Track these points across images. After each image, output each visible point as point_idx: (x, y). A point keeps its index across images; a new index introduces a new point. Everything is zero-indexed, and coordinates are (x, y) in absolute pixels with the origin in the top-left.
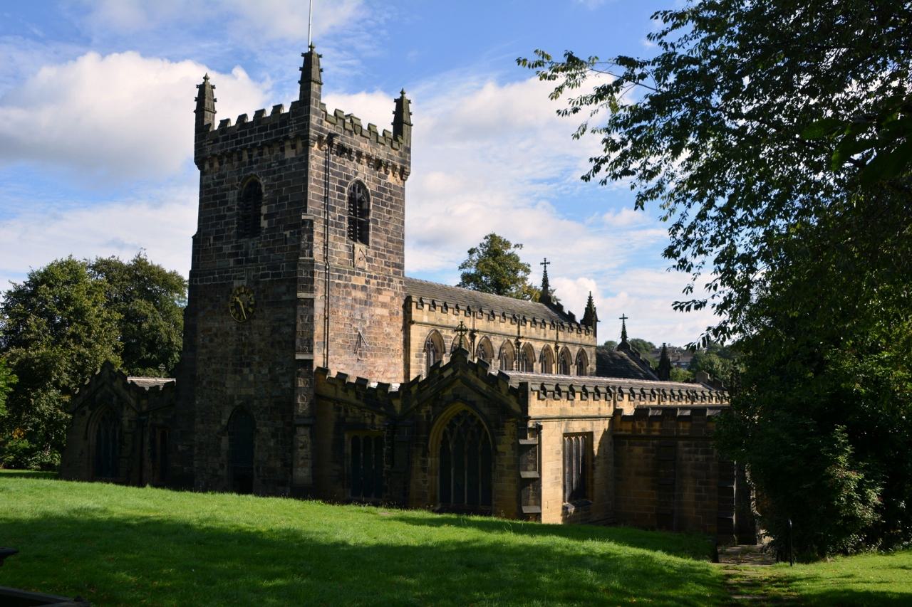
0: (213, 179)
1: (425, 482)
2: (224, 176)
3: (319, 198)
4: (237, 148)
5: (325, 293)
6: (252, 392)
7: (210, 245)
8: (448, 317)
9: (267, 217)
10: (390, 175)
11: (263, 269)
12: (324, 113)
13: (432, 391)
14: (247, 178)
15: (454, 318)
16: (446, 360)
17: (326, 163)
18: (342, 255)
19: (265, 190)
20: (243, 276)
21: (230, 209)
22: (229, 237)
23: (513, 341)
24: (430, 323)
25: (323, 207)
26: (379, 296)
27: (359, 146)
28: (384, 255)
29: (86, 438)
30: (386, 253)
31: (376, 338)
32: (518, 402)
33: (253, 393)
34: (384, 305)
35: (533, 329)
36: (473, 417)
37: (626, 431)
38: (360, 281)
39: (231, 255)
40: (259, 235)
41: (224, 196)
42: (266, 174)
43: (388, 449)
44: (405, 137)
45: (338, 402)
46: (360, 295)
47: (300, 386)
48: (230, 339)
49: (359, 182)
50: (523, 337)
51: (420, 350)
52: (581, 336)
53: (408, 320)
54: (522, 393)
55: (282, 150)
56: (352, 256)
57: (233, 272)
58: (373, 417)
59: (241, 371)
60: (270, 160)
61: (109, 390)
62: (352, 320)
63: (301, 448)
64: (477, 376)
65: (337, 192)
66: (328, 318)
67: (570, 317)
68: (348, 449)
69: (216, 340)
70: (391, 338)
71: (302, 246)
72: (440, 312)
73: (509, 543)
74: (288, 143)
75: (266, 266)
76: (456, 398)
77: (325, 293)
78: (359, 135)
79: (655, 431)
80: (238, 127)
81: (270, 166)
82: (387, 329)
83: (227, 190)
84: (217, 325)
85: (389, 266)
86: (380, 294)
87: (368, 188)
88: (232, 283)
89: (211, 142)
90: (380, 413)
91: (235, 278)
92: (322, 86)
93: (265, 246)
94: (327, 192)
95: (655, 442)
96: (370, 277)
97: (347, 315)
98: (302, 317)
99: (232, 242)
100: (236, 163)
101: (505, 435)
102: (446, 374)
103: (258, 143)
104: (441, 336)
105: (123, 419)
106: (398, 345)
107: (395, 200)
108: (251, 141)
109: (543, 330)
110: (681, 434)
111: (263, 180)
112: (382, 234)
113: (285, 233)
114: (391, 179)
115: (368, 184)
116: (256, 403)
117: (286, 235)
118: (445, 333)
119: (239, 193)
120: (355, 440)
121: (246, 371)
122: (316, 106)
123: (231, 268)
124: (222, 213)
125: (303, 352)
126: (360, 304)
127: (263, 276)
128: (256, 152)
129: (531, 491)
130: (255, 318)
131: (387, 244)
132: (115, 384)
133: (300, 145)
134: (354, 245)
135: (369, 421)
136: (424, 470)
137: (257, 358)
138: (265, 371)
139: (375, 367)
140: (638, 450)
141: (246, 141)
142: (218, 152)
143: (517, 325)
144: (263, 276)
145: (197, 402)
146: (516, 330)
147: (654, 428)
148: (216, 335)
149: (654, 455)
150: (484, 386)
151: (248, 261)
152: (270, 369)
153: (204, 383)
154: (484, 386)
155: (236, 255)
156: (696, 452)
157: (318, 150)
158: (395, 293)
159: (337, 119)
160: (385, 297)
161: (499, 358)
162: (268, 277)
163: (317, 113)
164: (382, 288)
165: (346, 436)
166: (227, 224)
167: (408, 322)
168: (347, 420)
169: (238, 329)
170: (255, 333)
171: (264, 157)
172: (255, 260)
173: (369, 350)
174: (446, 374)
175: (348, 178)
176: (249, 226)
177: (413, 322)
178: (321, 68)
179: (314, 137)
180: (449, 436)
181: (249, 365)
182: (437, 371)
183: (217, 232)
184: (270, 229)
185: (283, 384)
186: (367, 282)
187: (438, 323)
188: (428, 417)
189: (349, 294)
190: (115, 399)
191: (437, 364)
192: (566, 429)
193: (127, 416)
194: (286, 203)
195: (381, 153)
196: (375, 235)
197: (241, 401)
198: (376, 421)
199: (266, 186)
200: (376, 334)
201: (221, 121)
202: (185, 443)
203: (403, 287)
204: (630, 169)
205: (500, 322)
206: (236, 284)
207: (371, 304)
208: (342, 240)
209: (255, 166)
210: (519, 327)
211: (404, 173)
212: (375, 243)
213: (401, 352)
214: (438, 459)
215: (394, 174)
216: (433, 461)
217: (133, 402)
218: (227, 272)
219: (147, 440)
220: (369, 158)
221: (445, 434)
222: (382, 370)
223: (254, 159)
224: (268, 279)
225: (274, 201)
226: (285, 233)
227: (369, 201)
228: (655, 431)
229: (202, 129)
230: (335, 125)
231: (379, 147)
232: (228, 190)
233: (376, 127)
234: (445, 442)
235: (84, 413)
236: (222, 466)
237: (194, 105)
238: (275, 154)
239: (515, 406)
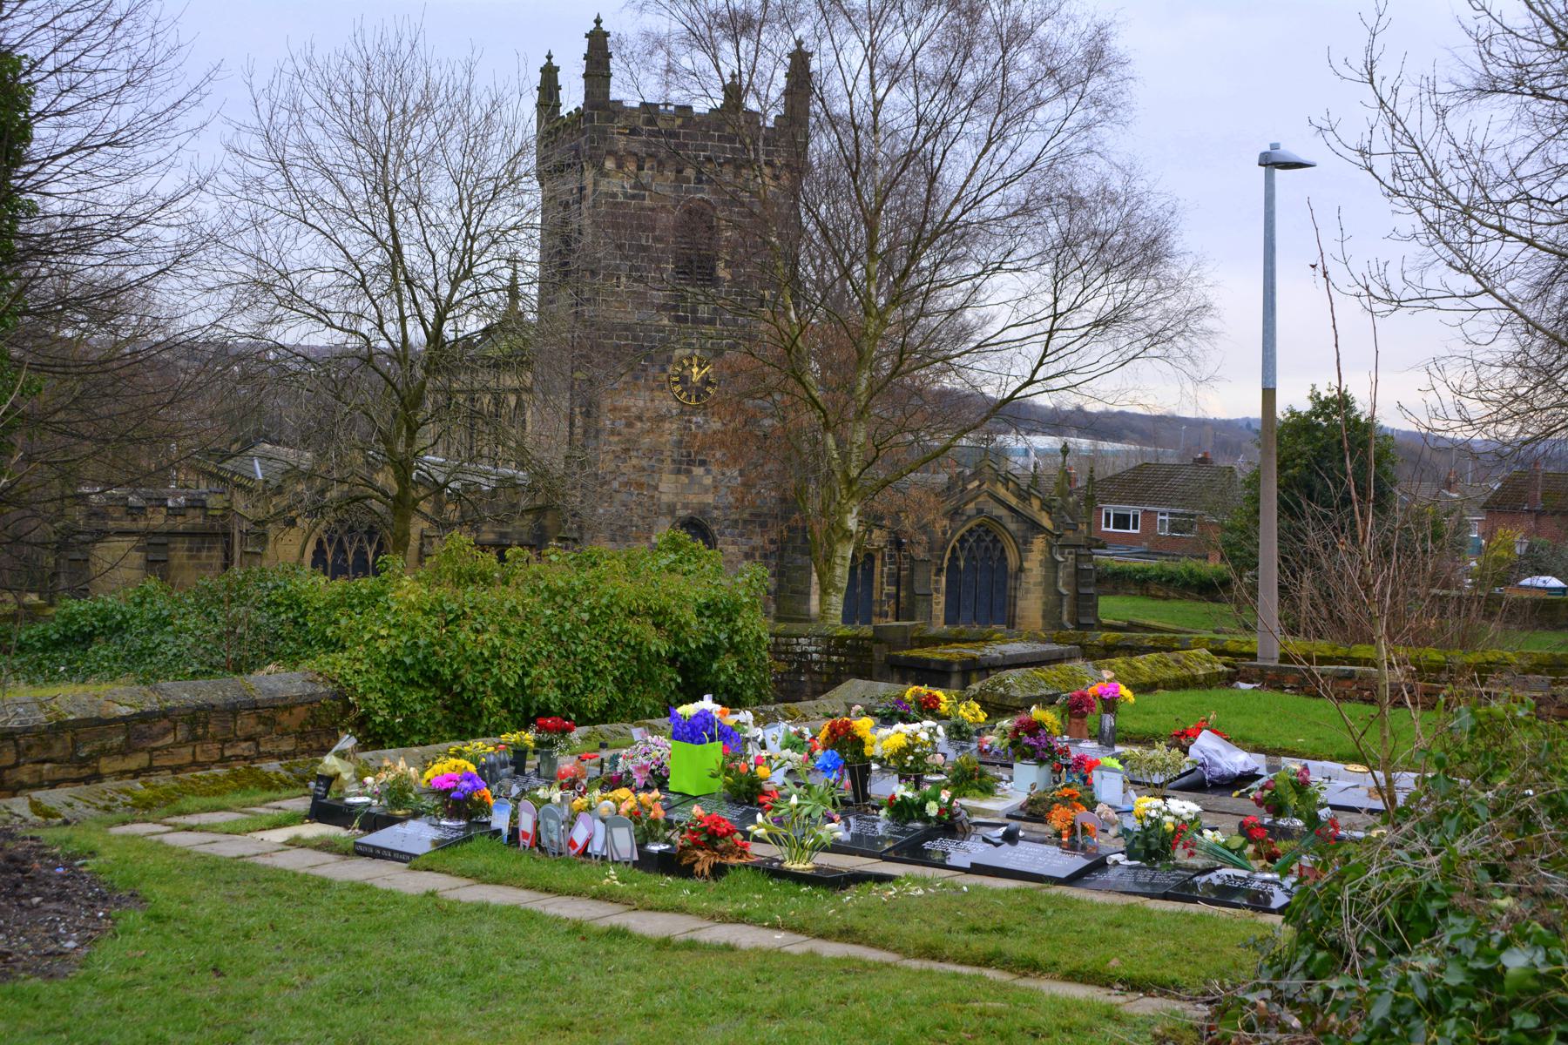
6: (709, 499)
39: (662, 307)
48: (667, 425)
59: (689, 472)
84: (641, 403)
116: (716, 513)
121: (698, 471)
155: (675, 308)
181: (703, 463)
188: (944, 533)
204: (1206, 1011)
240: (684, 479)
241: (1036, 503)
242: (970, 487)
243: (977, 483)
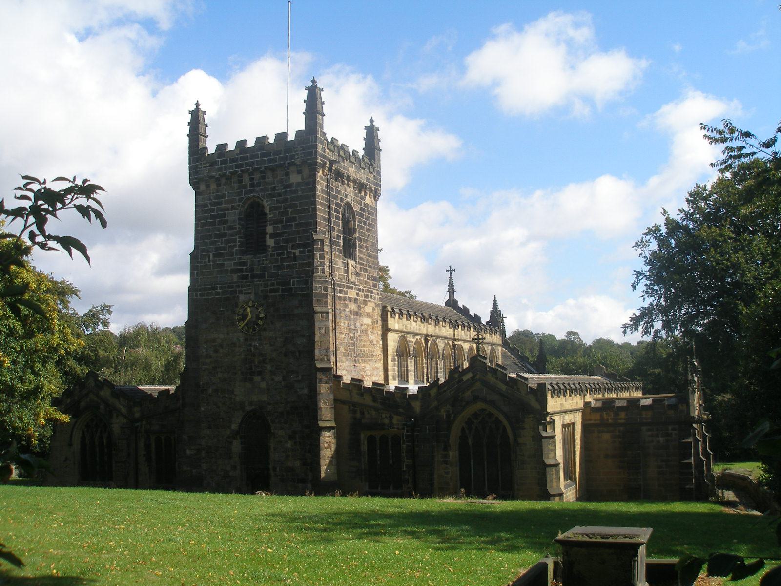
0: (210, 199)
1: (447, 473)
2: (223, 197)
3: (324, 219)
4: (238, 171)
5: (332, 306)
6: (264, 398)
7: (209, 261)
8: (411, 324)
9: (272, 236)
10: (367, 197)
11: (272, 284)
12: (325, 141)
13: (451, 393)
14: (249, 199)
15: (414, 324)
16: (466, 365)
17: (328, 187)
18: (340, 271)
19: (270, 211)
20: (250, 291)
21: (231, 228)
22: (231, 254)
23: (451, 343)
24: (400, 330)
25: (327, 227)
26: (366, 307)
27: (348, 171)
28: (366, 269)
29: (70, 445)
30: (367, 268)
31: (364, 345)
32: (537, 400)
33: (266, 399)
34: (369, 315)
35: (463, 331)
36: (490, 415)
37: (595, 420)
38: (352, 294)
39: (233, 271)
40: (263, 253)
41: (224, 215)
42: (271, 196)
43: (408, 446)
44: (377, 162)
45: (354, 405)
46: (353, 306)
47: (322, 391)
49: (348, 204)
50: (458, 340)
51: (394, 354)
52: (492, 337)
53: (385, 328)
54: (540, 393)
55: (287, 174)
56: (347, 272)
57: (238, 286)
58: (391, 418)
59: (251, 380)
60: (274, 183)
61: (95, 399)
62: (350, 329)
63: (326, 448)
64: (497, 378)
65: (335, 214)
66: (335, 329)
67: (476, 319)
68: (364, 447)
69: (221, 350)
70: (374, 345)
71: (315, 264)
72: (405, 319)
74: (292, 168)
75: (275, 282)
76: (476, 399)
77: (332, 306)
78: (348, 160)
79: (621, 419)
80: (238, 151)
81: (274, 189)
82: (371, 337)
83: (227, 210)
84: (222, 336)
85: (370, 280)
86: (366, 305)
87: (354, 208)
88: (238, 297)
89: (208, 165)
91: (241, 292)
92: (324, 117)
93: (273, 263)
94: (329, 214)
95: (621, 428)
96: (359, 290)
97: (346, 325)
98: (319, 328)
99: (235, 259)
100: (236, 185)
101: (525, 429)
102: (465, 378)
103: (261, 168)
104: (406, 340)
105: (113, 426)
106: (379, 351)
107: (370, 217)
108: (253, 165)
109: (468, 332)
110: (645, 421)
111: (267, 201)
112: (364, 251)
113: (293, 251)
114: (368, 200)
115: (354, 204)
116: (269, 408)
117: (295, 254)
118: (410, 338)
119: (240, 214)
120: (371, 440)
121: (257, 378)
122: (321, 136)
123: (235, 282)
124: (222, 232)
125: (322, 360)
126: (354, 315)
127: (272, 291)
128: (257, 176)
129: (554, 475)
130: (265, 329)
131: (368, 259)
132: (102, 393)
133: (306, 171)
134: (347, 262)
135: (386, 421)
136: (446, 463)
137: (269, 367)
138: (278, 378)
139: (365, 372)
141: (247, 165)
142: (216, 174)
143: (453, 329)
144: (272, 291)
145: (202, 409)
146: (452, 333)
147: (620, 417)
148: (221, 346)
149: (620, 440)
150: (503, 387)
151: (253, 277)
152: (283, 377)
153: (210, 391)
154: (503, 387)
155: (241, 271)
157: (322, 175)
158: (375, 303)
159: (334, 147)
160: (369, 309)
161: (442, 359)
162: (278, 292)
163: (321, 143)
164: (367, 300)
165: (362, 436)
166: (228, 241)
167: (386, 330)
168: (363, 421)
169: (246, 340)
170: (266, 344)
171: (267, 180)
172: (262, 276)
173: (361, 357)
174: (465, 378)
175: (342, 200)
176: (254, 242)
177: (390, 330)
178: (322, 100)
179: (320, 163)
180: (467, 431)
181: (260, 373)
182: (456, 376)
183: (217, 249)
184: (276, 248)
185: (298, 390)
186: (358, 295)
187: (405, 330)
188: (448, 416)
189: (346, 306)
190: (102, 407)
191: (457, 368)
192: (563, 422)
193: (117, 425)
194: (293, 223)
195: (362, 176)
196: (361, 252)
197: (253, 407)
198: (395, 421)
199: (270, 207)
200: (364, 341)
201: (217, 145)
202: (193, 448)
203: (380, 298)
205: (443, 326)
206: (242, 297)
208: (339, 257)
209: (257, 188)
210: (454, 330)
211: (376, 195)
212: (361, 258)
213: (381, 357)
214: (457, 452)
215: (370, 195)
216: (453, 454)
217: (124, 410)
218: (232, 287)
219: (141, 444)
220: (355, 181)
221: (463, 430)
222: (369, 374)
223: (255, 182)
224: (277, 294)
225: (281, 222)
226: (293, 251)
227: (355, 221)
230: (333, 152)
231: (361, 172)
232: (227, 210)
233: (358, 153)
234: (463, 438)
236: (234, 468)
237: (187, 129)
238: (279, 178)
239: (534, 403)
240: (248, 385)
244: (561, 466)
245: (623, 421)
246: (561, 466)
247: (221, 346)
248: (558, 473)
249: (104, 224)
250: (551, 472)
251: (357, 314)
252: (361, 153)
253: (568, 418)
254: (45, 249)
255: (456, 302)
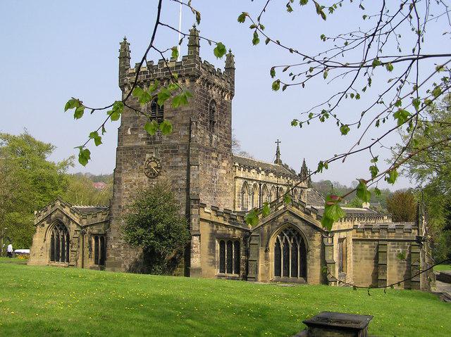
34: (224, 168)
46: (214, 162)
56: (211, 141)
73: (187, 300)
84: (135, 178)
90: (239, 229)
140: (366, 246)
151: (155, 143)
156: (398, 247)
160: (224, 164)
183: (134, 126)
188: (268, 231)
195: (223, 84)
207: (219, 168)
216: (272, 254)
228: (376, 236)
229: (123, 69)
235: (43, 225)
241: (314, 216)
242: (279, 208)
243: (283, 206)
244: (337, 264)
245: (377, 238)
246: (337, 264)
247: (135, 184)
248: (334, 267)
249: (325, 78)
250: (331, 267)
251: (217, 167)
252: (223, 70)
253: (343, 235)
254: (230, 68)
255: (281, 161)
